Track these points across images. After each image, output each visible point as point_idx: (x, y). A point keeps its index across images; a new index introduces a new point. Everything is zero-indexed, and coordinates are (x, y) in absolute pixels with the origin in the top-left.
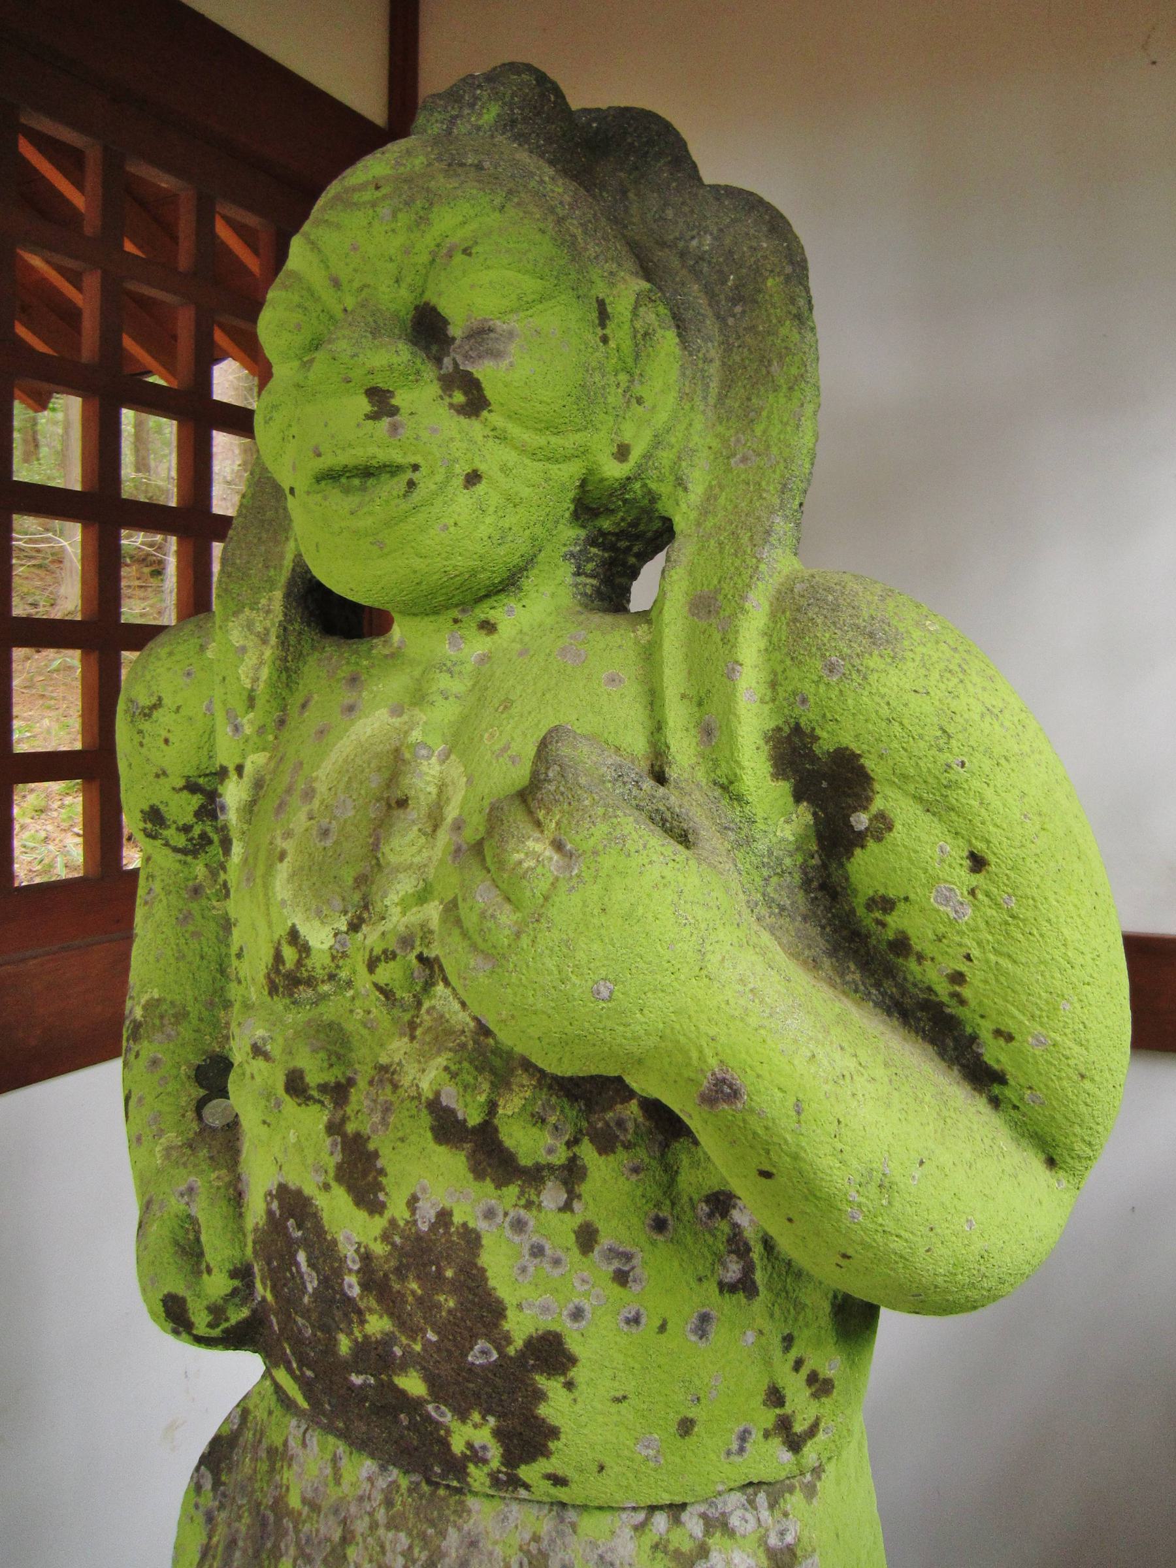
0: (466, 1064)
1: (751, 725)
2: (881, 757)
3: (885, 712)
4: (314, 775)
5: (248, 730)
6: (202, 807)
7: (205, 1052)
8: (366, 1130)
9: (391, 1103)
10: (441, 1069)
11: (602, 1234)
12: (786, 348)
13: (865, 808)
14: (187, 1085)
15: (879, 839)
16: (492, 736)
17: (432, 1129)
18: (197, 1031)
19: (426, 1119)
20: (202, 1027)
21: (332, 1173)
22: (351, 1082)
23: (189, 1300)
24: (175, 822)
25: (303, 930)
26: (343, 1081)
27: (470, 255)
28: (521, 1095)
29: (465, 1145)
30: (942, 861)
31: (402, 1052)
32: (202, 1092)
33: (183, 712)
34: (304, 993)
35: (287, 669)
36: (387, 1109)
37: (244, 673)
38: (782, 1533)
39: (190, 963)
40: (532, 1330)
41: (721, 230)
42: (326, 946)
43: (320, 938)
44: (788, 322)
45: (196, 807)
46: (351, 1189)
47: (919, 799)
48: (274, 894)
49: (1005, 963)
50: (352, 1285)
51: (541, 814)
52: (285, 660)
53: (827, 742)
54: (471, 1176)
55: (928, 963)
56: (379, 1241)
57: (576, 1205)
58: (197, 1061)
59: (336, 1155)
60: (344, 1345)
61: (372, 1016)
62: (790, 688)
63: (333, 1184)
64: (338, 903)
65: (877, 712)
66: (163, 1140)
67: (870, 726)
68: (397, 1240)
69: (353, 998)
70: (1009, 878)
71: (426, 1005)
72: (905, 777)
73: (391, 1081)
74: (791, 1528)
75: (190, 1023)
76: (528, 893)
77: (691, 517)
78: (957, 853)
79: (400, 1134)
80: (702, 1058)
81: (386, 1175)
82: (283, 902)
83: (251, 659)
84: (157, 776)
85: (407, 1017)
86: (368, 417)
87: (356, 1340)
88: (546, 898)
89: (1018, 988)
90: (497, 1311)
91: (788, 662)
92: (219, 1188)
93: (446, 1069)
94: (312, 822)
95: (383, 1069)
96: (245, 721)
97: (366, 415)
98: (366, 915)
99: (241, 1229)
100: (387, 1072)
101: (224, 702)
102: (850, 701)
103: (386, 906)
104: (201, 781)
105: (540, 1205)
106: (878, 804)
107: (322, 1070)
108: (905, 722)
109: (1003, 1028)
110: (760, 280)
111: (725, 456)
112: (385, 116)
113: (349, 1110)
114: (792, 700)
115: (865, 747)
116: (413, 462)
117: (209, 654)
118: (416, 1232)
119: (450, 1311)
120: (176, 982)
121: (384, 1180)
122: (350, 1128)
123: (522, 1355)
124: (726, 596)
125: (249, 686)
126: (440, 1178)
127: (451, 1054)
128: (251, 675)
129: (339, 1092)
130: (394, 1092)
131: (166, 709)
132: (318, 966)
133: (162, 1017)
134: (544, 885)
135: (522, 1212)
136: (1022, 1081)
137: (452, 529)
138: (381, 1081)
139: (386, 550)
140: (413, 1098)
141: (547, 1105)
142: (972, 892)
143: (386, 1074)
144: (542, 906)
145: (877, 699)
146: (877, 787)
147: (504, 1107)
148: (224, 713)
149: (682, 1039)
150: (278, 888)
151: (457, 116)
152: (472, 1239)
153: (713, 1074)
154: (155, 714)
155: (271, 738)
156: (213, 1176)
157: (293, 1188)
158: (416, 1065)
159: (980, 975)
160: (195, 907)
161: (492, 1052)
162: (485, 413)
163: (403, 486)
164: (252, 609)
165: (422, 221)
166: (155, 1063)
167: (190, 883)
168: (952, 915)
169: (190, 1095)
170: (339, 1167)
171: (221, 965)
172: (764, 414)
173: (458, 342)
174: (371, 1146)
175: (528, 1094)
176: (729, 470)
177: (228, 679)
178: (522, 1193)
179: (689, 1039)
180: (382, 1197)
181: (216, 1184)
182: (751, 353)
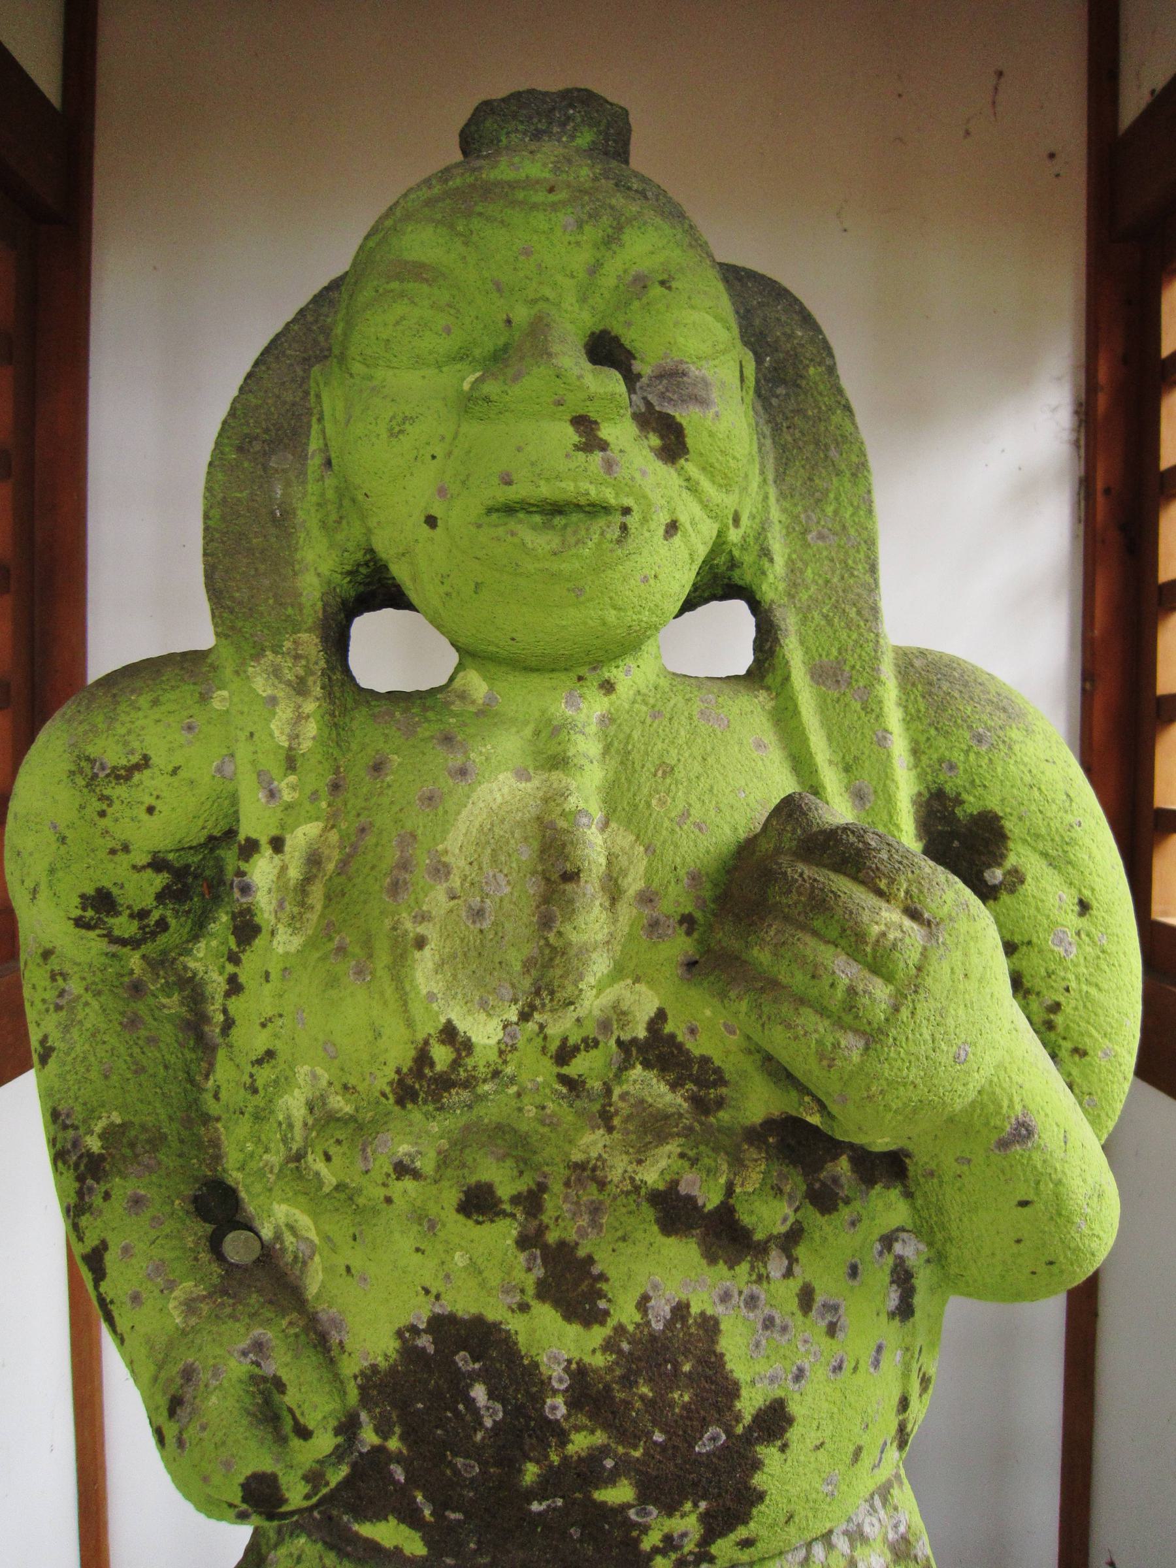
0: (702, 1148)
1: (905, 789)
2: (1020, 818)
3: (1028, 779)
4: (440, 847)
5: (287, 796)
6: (167, 887)
7: (196, 1179)
8: (572, 1235)
9: (601, 1202)
10: (674, 1156)
11: (817, 1291)
12: (842, 436)
13: (1000, 865)
14: (188, 1222)
15: (1012, 891)
16: (662, 802)
17: (657, 1221)
18: (180, 1156)
19: (648, 1213)
20: (185, 1150)
21: (531, 1290)
22: (542, 1188)
23: (280, 1474)
24: (129, 907)
25: (462, 1026)
26: (534, 1187)
27: (669, 288)
28: (758, 1169)
29: (694, 1232)
30: (1060, 907)
31: (600, 1145)
32: (209, 1228)
33: (182, 774)
34: (458, 1096)
35: (336, 725)
36: (596, 1210)
37: (279, 727)
38: (896, 1526)
39: (154, 1076)
40: (761, 1402)
41: (748, 311)
42: (493, 1041)
43: (484, 1033)
44: (839, 412)
45: (159, 889)
46: (557, 1304)
47: (1045, 855)
48: (415, 988)
49: (1093, 991)
50: (557, 1407)
51: (883, 884)
52: (333, 715)
53: (972, 805)
54: (704, 1262)
55: (1033, 997)
56: (598, 1353)
57: (797, 1269)
58: (189, 1192)
59: (535, 1271)
60: (531, 1472)
61: (548, 1111)
62: (935, 756)
63: (534, 1303)
64: (507, 993)
65: (1022, 779)
66: (176, 1293)
67: (1015, 791)
68: (625, 1346)
69: (519, 1095)
70: (1104, 919)
71: (617, 1091)
72: (1037, 836)
73: (594, 1179)
74: (902, 1519)
75: (170, 1147)
76: (902, 965)
77: (780, 588)
78: (1070, 901)
79: (620, 1234)
80: (1011, 1106)
81: (607, 1280)
82: (431, 997)
83: (284, 713)
84: (113, 852)
85: (596, 1107)
86: (577, 448)
87: (551, 1466)
88: (919, 969)
89: (1099, 1011)
90: (732, 1391)
91: (933, 732)
92: (297, 1336)
93: (682, 1156)
95: (580, 1167)
96: (283, 785)
97: (575, 445)
98: (538, 1002)
99: (337, 1377)
101: (253, 762)
102: (999, 770)
103: (581, 990)
104: (171, 856)
105: (768, 1277)
106: (1011, 860)
107: (513, 1179)
108: (1043, 787)
109: (1080, 1046)
110: (801, 367)
111: (798, 531)
113: (545, 1218)
114: (937, 767)
115: (1008, 810)
116: (626, 505)
117: (216, 704)
118: (650, 1334)
119: (685, 1407)
120: (142, 1102)
121: (604, 1286)
122: (552, 1237)
123: (749, 1429)
124: (853, 667)
125: (286, 744)
126: (674, 1271)
127: (682, 1140)
128: (287, 731)
129: (532, 1201)
130: (601, 1191)
131: (156, 770)
132: (482, 1063)
133: (132, 1145)
134: (914, 956)
135: (754, 1287)
136: (1085, 1089)
137: (652, 581)
139: (582, 599)
140: (628, 1193)
141: (783, 1177)
142: (1078, 934)
143: (586, 1173)
144: (917, 977)
145: (1022, 767)
146: (1011, 845)
147: (742, 1185)
148: (254, 776)
149: (998, 1090)
151: (544, 132)
152: (710, 1326)
153: (1017, 1119)
154: (137, 777)
155: (324, 805)
156: (284, 1323)
157: (466, 1317)
158: (624, 1157)
159: (1073, 1003)
160: (141, 1008)
161: (719, 1131)
162: (682, 461)
163: (614, 533)
164: (275, 652)
165: (611, 240)
166: (137, 1202)
167: (126, 979)
168: (1063, 954)
169: (196, 1234)
170: (541, 1284)
171: (188, 1073)
172: (832, 495)
173: (644, 380)
174: (581, 1253)
175: (763, 1167)
176: (806, 545)
177: (256, 736)
178: (752, 1268)
179: (1003, 1089)
180: (602, 1304)
181: (292, 1331)
182: (803, 435)
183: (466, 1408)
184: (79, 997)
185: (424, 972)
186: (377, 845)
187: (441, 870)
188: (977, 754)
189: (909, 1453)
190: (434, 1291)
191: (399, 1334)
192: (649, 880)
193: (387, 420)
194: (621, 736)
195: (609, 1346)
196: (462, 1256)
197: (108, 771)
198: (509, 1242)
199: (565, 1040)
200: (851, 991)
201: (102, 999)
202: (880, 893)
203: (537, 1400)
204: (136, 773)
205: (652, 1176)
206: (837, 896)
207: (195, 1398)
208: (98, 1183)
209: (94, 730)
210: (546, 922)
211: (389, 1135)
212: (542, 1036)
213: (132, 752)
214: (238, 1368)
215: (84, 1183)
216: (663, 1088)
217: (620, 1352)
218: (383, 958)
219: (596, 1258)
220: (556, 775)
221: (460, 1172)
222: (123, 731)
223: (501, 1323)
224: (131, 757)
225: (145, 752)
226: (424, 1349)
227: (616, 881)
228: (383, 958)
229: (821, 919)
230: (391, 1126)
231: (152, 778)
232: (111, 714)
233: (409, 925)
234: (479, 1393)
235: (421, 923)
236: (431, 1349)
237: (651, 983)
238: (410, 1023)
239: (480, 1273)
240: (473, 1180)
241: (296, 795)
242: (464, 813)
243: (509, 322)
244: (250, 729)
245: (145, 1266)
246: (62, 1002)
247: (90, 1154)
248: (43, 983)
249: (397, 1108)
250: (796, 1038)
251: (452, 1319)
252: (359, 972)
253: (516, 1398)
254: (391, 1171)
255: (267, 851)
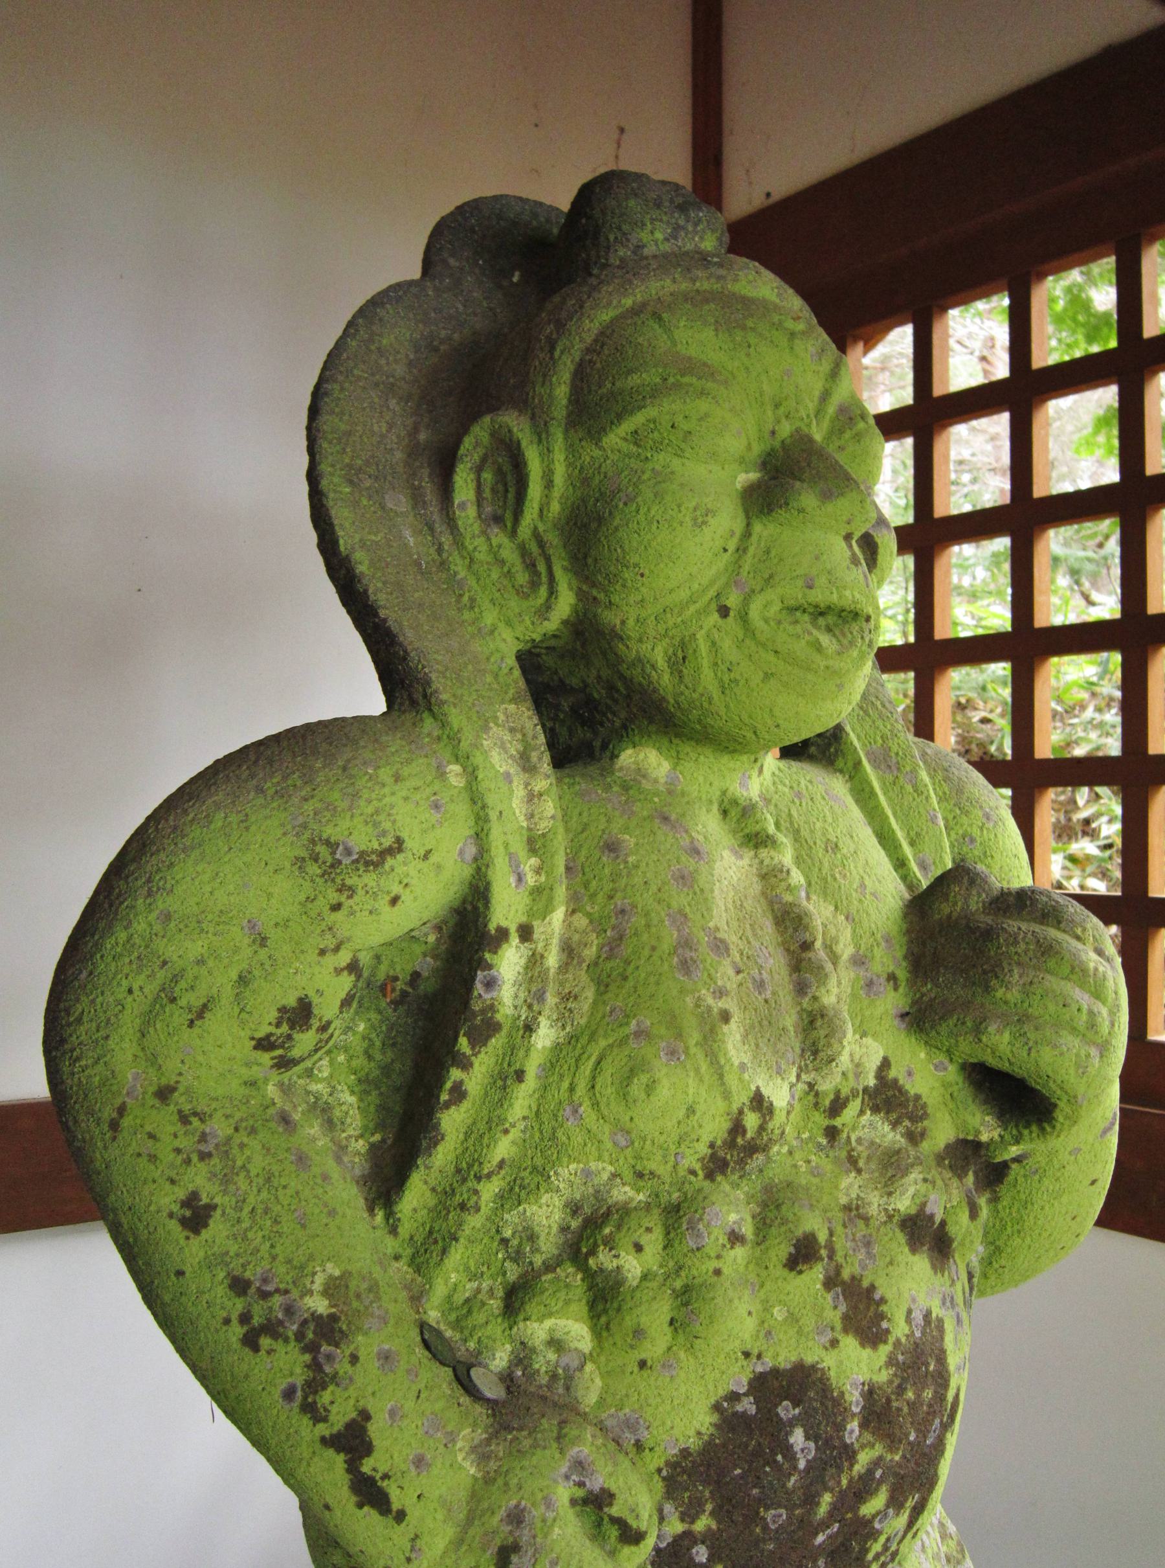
8: (857, 1270)
21: (839, 1326)
31: (856, 1186)
33: (433, 859)
48: (728, 1060)
51: (1079, 931)
61: (813, 1164)
62: (961, 832)
66: (459, 1444)
69: (790, 1153)
73: (860, 1217)
82: (743, 1067)
91: (958, 812)
93: (925, 1180)
94: (741, 975)
95: (847, 1208)
100: (850, 1210)
101: (506, 845)
112: (986, 295)
121: (884, 1308)
122: (846, 1274)
124: (897, 754)
127: (920, 1168)
130: (867, 1225)
138: (850, 1220)
140: (885, 1223)
150: (732, 1053)
154: (390, 862)
157: (789, 1366)
158: (876, 1193)
166: (386, 1358)
170: (846, 1318)
180: (884, 1325)
183: (784, 1457)
184: (229, 1139)
185: (734, 1044)
186: (648, 926)
187: (720, 947)
188: (988, 829)
189: (959, 1434)
190: (755, 1352)
191: (717, 1407)
192: (857, 947)
193: (691, 510)
194: (784, 816)
195: (891, 1361)
196: (780, 1311)
197: (355, 857)
198: (818, 1286)
199: (838, 1093)
200: (1091, 1013)
201: (260, 1136)
202: (1078, 938)
203: (840, 1427)
204: (389, 858)
205: (904, 1204)
206: (1059, 943)
207: (534, 1537)
208: (337, 1346)
209: (331, 807)
210: (801, 989)
211: (717, 1208)
212: (813, 1093)
213: (384, 833)
214: (563, 1493)
215: (319, 1352)
216: (887, 1128)
217: (897, 1365)
218: (694, 1037)
219: (877, 1285)
220: (764, 853)
221: (783, 1229)
222: (370, 810)
223: (818, 1363)
224: (383, 840)
225: (398, 834)
226: (744, 1413)
227: (831, 948)
228: (694, 1037)
229: (1054, 960)
230: (714, 1199)
231: (405, 864)
232: (350, 790)
233: (710, 1001)
234: (798, 1438)
235: (720, 998)
236: (752, 1410)
237: (875, 1036)
238: (727, 1096)
239: (797, 1321)
240: (799, 1233)
241: (543, 879)
242: (716, 892)
243: (773, 433)
244: (498, 809)
245: (420, 1423)
246: (209, 1147)
247: (316, 1318)
248: (171, 1129)
249: (707, 1183)
250: (1062, 1054)
251: (775, 1372)
252: (672, 1053)
253: (826, 1432)
254: (726, 1242)
255: (514, 939)
